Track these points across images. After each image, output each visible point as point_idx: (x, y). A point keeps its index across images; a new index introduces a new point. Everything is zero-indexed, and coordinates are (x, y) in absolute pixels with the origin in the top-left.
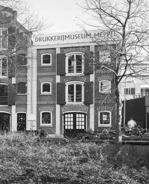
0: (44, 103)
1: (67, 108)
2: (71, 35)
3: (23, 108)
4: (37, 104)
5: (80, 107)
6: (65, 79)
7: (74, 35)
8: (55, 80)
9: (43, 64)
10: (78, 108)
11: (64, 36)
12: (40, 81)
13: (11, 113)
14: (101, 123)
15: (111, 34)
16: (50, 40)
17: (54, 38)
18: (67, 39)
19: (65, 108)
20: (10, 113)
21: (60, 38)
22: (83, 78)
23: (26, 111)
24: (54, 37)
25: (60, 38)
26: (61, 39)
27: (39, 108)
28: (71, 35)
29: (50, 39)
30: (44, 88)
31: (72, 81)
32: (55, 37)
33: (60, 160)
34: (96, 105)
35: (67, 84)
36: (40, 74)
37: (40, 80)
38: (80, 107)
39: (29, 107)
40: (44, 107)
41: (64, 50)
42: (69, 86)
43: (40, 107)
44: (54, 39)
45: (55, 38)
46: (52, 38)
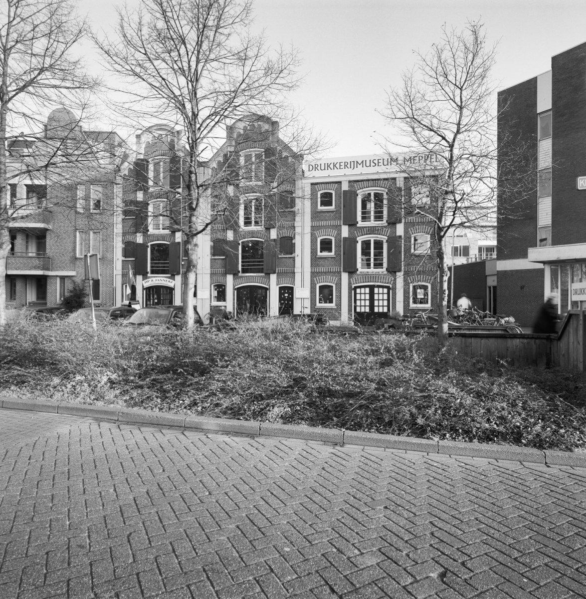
0: (323, 269)
4: (311, 272)
6: (355, 232)
8: (340, 234)
9: (320, 208)
14: (415, 302)
16: (332, 168)
17: (338, 166)
18: (360, 167)
20: (268, 287)
21: (349, 166)
23: (294, 283)
24: (338, 164)
25: (349, 166)
29: (332, 166)
31: (367, 234)
34: (407, 274)
35: (360, 239)
36: (316, 224)
37: (317, 233)
43: (315, 277)
44: (338, 167)
45: (340, 166)
46: (334, 166)
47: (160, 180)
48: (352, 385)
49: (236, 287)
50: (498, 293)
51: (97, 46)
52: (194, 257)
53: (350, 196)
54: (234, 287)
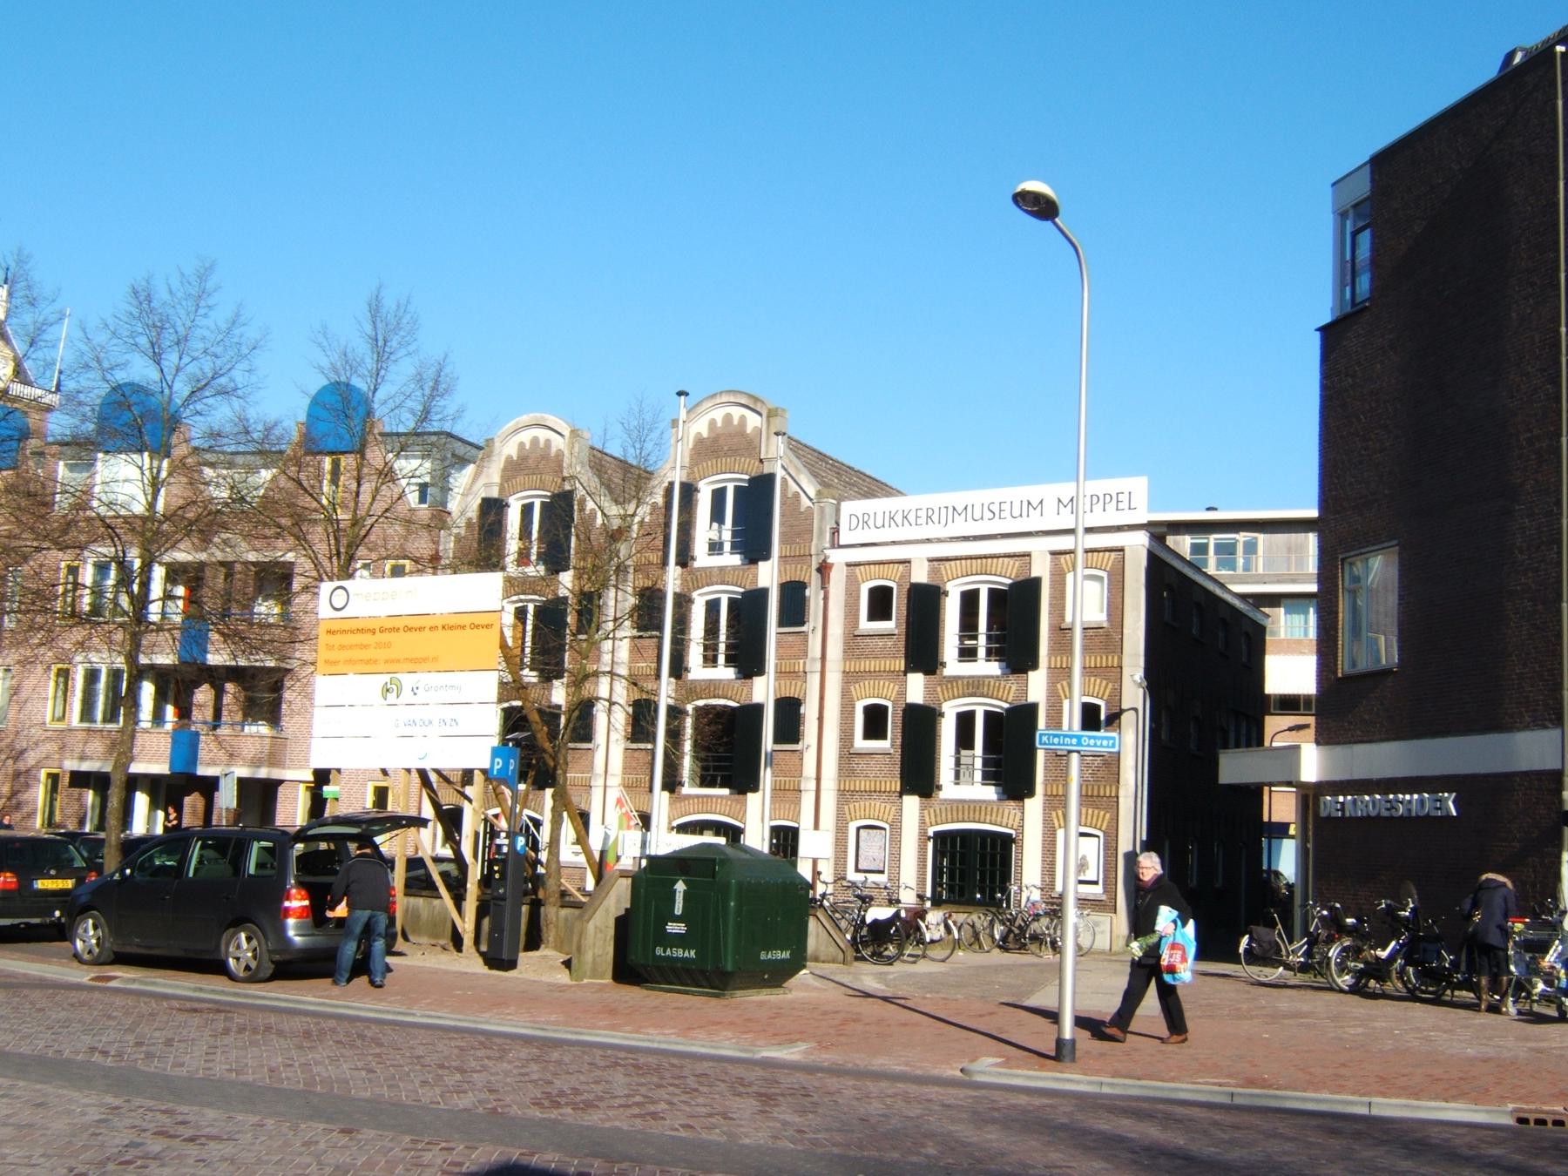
0: (863, 785)
8: (903, 693)
9: (865, 625)
14: (857, 870)
18: (959, 519)
23: (797, 819)
25: (935, 518)
29: (899, 518)
30: (411, 874)
33: (243, 639)
35: (950, 711)
37: (854, 690)
39: (808, 800)
43: (847, 802)
44: (912, 520)
46: (905, 517)
47: (544, 751)
48: (73, 571)
49: (675, 824)
50: (179, 953)
51: (368, 328)
53: (925, 601)
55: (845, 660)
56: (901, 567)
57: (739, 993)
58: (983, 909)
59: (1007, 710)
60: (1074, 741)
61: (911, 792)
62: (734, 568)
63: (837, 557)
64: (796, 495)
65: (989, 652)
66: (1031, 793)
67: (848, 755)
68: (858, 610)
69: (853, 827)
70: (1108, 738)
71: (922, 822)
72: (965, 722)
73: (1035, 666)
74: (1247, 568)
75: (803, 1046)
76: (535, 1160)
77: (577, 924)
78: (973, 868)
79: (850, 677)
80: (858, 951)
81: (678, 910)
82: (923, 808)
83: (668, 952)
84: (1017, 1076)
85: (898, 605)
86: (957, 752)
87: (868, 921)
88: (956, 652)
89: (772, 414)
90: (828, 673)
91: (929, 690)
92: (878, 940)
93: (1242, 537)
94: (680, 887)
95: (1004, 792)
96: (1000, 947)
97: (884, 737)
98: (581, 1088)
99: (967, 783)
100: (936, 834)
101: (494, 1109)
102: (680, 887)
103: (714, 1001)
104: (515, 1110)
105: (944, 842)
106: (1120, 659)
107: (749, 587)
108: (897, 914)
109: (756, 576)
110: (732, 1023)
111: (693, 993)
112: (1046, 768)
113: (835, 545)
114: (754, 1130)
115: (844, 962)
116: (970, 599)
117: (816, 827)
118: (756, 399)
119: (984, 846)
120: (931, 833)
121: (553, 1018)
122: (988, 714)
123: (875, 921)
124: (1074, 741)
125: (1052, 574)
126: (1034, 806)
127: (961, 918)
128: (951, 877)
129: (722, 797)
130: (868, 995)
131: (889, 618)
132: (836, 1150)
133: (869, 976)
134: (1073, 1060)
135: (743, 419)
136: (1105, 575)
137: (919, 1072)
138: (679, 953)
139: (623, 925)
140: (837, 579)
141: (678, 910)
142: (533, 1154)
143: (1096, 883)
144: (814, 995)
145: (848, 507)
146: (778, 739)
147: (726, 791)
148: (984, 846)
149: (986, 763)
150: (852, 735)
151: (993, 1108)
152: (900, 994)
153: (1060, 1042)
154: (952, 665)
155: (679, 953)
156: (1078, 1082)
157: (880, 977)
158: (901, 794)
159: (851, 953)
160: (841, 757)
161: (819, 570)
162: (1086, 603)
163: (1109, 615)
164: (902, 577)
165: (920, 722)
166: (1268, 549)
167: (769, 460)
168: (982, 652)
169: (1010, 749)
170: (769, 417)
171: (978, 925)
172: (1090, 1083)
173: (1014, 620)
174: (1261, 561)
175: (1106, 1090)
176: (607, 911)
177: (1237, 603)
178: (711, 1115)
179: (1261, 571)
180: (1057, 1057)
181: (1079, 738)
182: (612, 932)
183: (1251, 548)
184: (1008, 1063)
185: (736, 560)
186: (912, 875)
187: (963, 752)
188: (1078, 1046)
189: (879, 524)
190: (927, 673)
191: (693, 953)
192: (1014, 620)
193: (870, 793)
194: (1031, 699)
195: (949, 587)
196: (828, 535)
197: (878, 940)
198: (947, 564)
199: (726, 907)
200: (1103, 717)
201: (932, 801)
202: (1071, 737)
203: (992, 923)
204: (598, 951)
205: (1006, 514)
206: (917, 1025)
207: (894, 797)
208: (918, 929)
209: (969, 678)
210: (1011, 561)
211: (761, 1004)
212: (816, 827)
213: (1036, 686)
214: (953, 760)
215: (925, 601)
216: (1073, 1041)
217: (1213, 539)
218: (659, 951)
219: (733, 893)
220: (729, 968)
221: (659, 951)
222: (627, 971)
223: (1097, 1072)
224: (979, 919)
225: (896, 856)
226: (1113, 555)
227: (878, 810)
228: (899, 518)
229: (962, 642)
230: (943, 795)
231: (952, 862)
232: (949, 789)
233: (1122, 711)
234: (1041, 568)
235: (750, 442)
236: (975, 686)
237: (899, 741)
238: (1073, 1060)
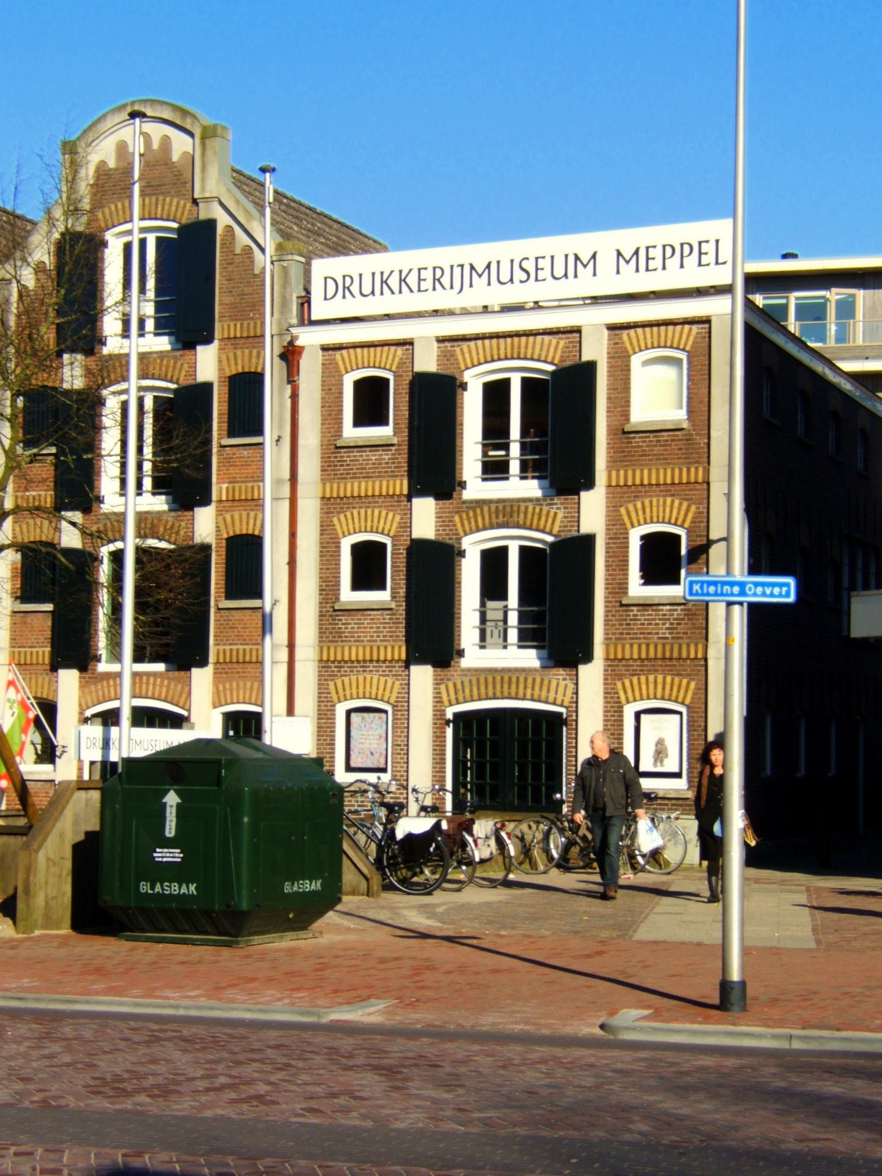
0: (354, 652)
1: (467, 684)
2: (498, 262)
3: (249, 684)
4: (321, 661)
5: (530, 680)
6: (457, 518)
7: (512, 261)
8: (407, 525)
9: (351, 432)
10: (521, 686)
11: (462, 266)
12: (338, 527)
13: (189, 711)
14: (349, 769)
15: (700, 254)
16: (396, 289)
17: (412, 280)
19: (459, 686)
20: (185, 713)
21: (446, 281)
22: (548, 512)
24: (415, 273)
25: (446, 281)
26: (447, 285)
27: (331, 684)
28: (498, 262)
29: (394, 282)
31: (492, 527)
32: (419, 270)
34: (616, 669)
35: (473, 547)
36: (334, 489)
38: (530, 680)
40: (354, 678)
41: (458, 349)
42: (112, 554)
43: (333, 676)
44: (414, 285)
45: (420, 280)
46: (402, 280)
49: (88, 713)
52: (435, 893)
53: (435, 396)
54: (81, 713)
55: (324, 481)
56: (400, 351)
57: (257, 939)
58: (537, 816)
59: (552, 545)
60: (736, 589)
61: (422, 660)
62: (162, 355)
63: (310, 339)
64: (248, 251)
65: (524, 467)
66: (588, 657)
67: (331, 613)
68: (340, 411)
69: (341, 710)
70: (781, 585)
71: (438, 700)
72: (493, 561)
73: (590, 484)
74: (841, 337)
75: (381, 1005)
76: (147, 1161)
77: (23, 858)
78: (507, 758)
79: (332, 506)
80: (384, 876)
81: (170, 830)
82: (438, 682)
83: (158, 888)
84: (678, 1031)
85: (397, 403)
86: (483, 604)
87: (399, 835)
88: (479, 466)
89: (209, 134)
90: (294, 497)
91: (442, 520)
92: (407, 862)
93: (834, 295)
94: (172, 799)
95: (551, 657)
96: (558, 866)
97: (383, 587)
98: (141, 1069)
99: (495, 646)
100: (456, 715)
101: (44, 1101)
102: (172, 799)
103: (226, 952)
104: (71, 1102)
105: (466, 724)
106: (707, 472)
107: (184, 382)
108: (437, 825)
109: (194, 366)
110: (270, 980)
111: (193, 943)
112: (607, 622)
113: (306, 320)
114: (409, 1113)
115: (368, 893)
116: (496, 394)
117: (290, 711)
118: (185, 113)
119: (523, 730)
120: (449, 716)
121: (26, 982)
122: (523, 550)
123: (409, 837)
124: (736, 589)
125: (611, 357)
126: (591, 675)
127: (510, 826)
128: (480, 773)
129: (155, 674)
130: (424, 936)
131: (383, 421)
132: (522, 1131)
133: (409, 909)
134: (744, 1008)
135: (166, 141)
136: (683, 356)
137: (546, 1032)
138: (174, 889)
139: (87, 854)
140: (310, 370)
141: (170, 830)
142: (140, 1154)
143: (678, 775)
144: (351, 937)
145: (322, 267)
146: (232, 592)
147: (160, 667)
148: (523, 730)
149: (523, 617)
150: (337, 584)
151: (671, 1070)
152: (465, 932)
153: (725, 986)
154: (475, 486)
155: (174, 889)
156: (759, 1036)
157: (425, 909)
158: (407, 664)
159: (376, 880)
160: (322, 615)
161: (284, 356)
162: (655, 395)
163: (690, 412)
164: (401, 364)
165: (432, 566)
166: (871, 311)
167: (207, 200)
168: (515, 467)
169: (556, 600)
170: (203, 139)
171: (528, 838)
172: (774, 1037)
173: (558, 419)
174: (860, 327)
175: (797, 1045)
176: (62, 836)
177: (847, 386)
178: (334, 1095)
179: (860, 341)
180: (724, 1005)
181: (742, 585)
182: (68, 864)
183: (846, 310)
184: (657, 1015)
185: (163, 343)
186: (425, 768)
187: (490, 604)
188: (750, 992)
189: (367, 289)
190: (438, 497)
191: (192, 888)
192: (558, 419)
193: (363, 664)
194: (585, 529)
195: (468, 376)
196: (294, 308)
197: (407, 862)
198: (465, 345)
199: (238, 823)
200: (683, 551)
201: (451, 672)
202: (732, 584)
203: (547, 835)
204: (52, 892)
205: (545, 274)
206: (510, 970)
207: (398, 668)
208: (464, 845)
209: (498, 500)
210: (554, 340)
211: (291, 952)
212: (290, 711)
213: (592, 511)
214: (477, 615)
215: (435, 396)
216: (743, 984)
217: (794, 298)
218: (144, 887)
219: (247, 806)
220: (245, 906)
221: (144, 887)
222: (93, 913)
223: (781, 1023)
224: (531, 829)
225: (403, 749)
226: (695, 328)
227: (377, 686)
228: (394, 282)
229: (485, 454)
230: (465, 663)
231: (480, 753)
232: (474, 655)
233: (710, 543)
234: (594, 349)
235: (179, 174)
236: (506, 513)
237: (402, 592)
238: (744, 1008)
